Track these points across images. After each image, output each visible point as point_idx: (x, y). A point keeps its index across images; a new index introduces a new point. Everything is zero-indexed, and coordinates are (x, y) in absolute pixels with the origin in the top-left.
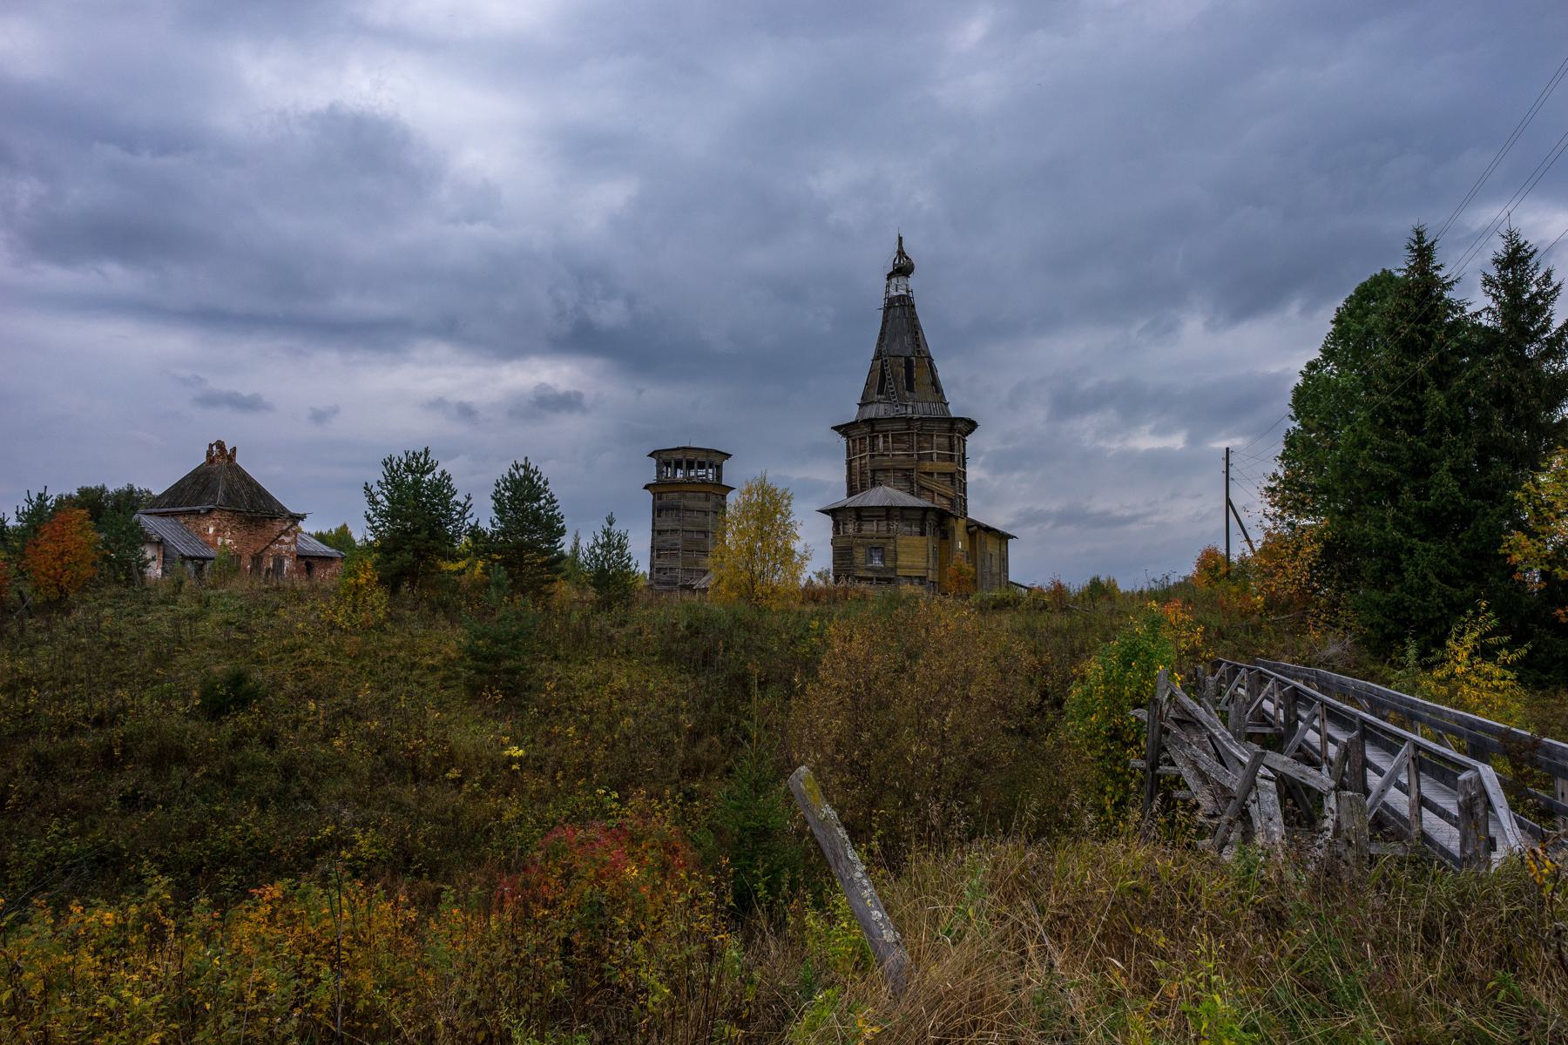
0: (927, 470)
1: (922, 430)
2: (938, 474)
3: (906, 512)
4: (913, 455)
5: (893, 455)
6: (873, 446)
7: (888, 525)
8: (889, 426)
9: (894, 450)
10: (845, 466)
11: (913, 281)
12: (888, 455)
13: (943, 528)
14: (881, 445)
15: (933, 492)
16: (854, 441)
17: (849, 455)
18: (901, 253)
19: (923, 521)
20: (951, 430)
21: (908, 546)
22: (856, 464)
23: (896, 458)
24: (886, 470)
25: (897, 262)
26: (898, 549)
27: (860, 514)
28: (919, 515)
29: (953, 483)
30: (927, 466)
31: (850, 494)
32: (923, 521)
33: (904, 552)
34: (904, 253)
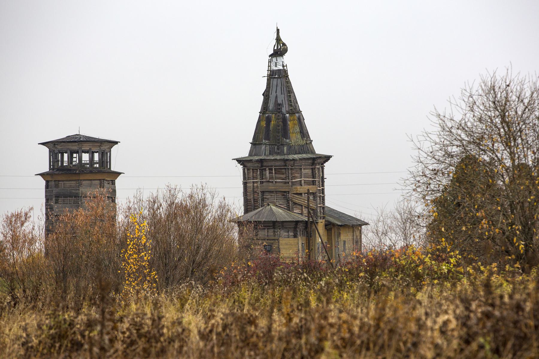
0: (298, 192)
3: (285, 224)
4: (288, 183)
6: (262, 176)
7: (274, 232)
8: (272, 163)
9: (276, 178)
10: (242, 186)
11: (287, 59)
12: (273, 182)
14: (268, 174)
15: (302, 206)
16: (248, 169)
17: (244, 178)
18: (278, 40)
19: (295, 229)
20: (313, 164)
21: (287, 244)
22: (250, 185)
23: (277, 184)
25: (276, 48)
26: (281, 247)
27: (257, 224)
28: (293, 225)
30: (300, 189)
31: (246, 211)
32: (295, 229)
33: (284, 248)
34: (280, 40)
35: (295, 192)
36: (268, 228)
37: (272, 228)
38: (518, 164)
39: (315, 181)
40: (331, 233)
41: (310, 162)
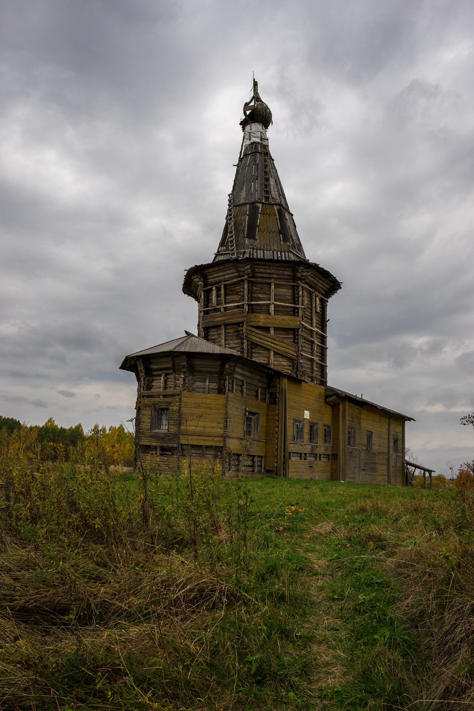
0: (261, 324)
1: (253, 277)
2: (276, 329)
3: (197, 362)
5: (226, 309)
13: (272, 390)
15: (269, 350)
18: (256, 98)
24: (218, 327)
26: (184, 410)
29: (296, 341)
30: (262, 319)
35: (254, 324)
36: (167, 372)
37: (171, 371)
38: (225, 692)
39: (298, 308)
40: (338, 411)
41: (286, 273)
